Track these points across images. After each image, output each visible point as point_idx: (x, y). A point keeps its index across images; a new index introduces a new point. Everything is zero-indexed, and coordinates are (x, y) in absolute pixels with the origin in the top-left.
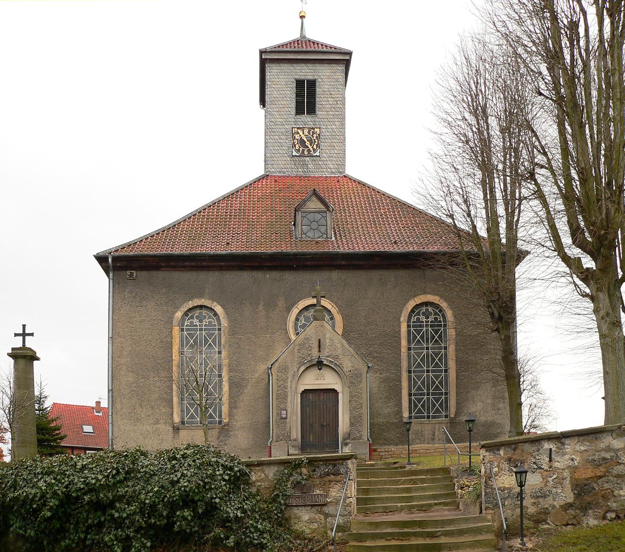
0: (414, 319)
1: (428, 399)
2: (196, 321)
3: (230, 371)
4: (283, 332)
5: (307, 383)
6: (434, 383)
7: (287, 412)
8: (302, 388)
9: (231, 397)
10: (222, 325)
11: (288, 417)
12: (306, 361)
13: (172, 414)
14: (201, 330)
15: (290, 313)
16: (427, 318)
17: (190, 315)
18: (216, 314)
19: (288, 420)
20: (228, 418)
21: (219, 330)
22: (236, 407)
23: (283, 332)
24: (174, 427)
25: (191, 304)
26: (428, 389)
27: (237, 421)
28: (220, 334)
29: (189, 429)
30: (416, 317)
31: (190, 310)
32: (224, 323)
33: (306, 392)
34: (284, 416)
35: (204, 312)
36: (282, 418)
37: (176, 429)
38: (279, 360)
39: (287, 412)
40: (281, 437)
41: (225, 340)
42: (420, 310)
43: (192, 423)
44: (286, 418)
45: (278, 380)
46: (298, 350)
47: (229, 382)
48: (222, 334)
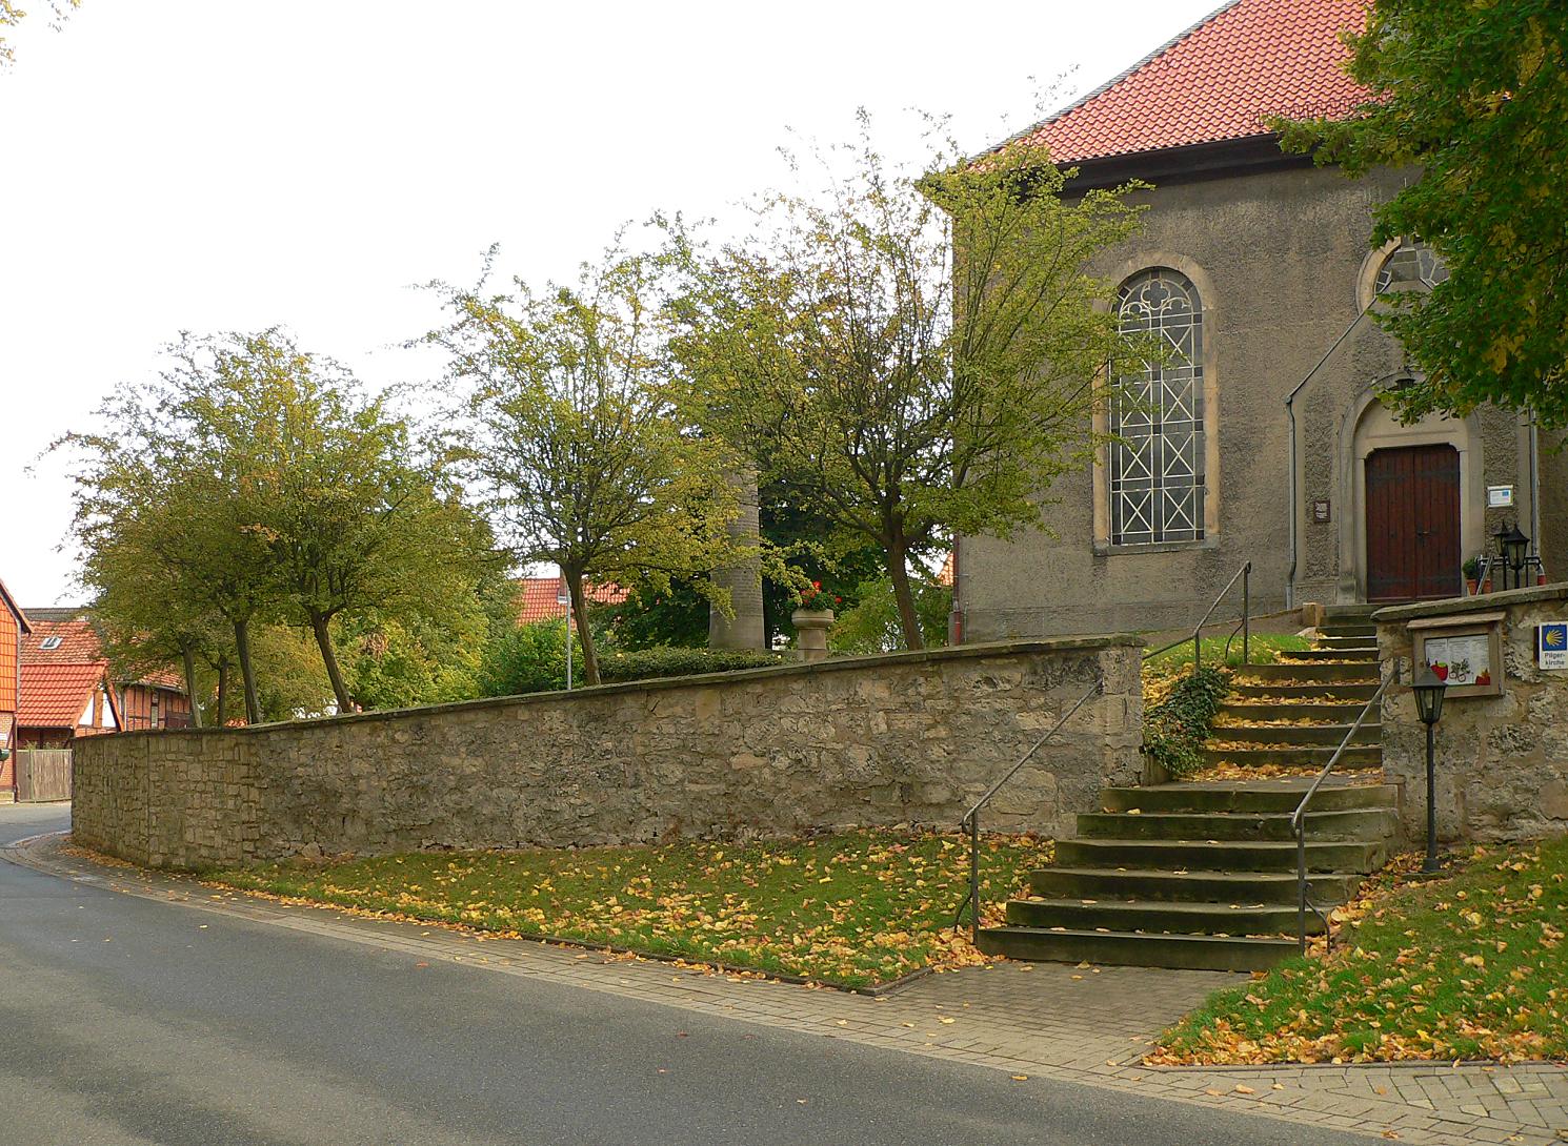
0: (1126, 310)
1: (1158, 493)
2: (1145, 306)
3: (1223, 412)
4: (1348, 311)
5: (1382, 433)
6: (1170, 455)
7: (1329, 506)
8: (1367, 447)
9: (1224, 474)
10: (1204, 309)
11: (1333, 517)
12: (1374, 382)
13: (1091, 522)
14: (1156, 323)
15: (1364, 263)
16: (1156, 304)
17: (1131, 292)
18: (1188, 284)
19: (1332, 524)
20: (1217, 524)
21: (1198, 319)
22: (1236, 498)
23: (1348, 311)
24: (1094, 552)
25: (1130, 268)
26: (1158, 473)
27: (1239, 531)
28: (1198, 330)
29: (1129, 552)
30: (1129, 305)
31: (1131, 280)
32: (1208, 305)
33: (1376, 455)
34: (1322, 516)
35: (1163, 282)
36: (1317, 521)
37: (1101, 557)
38: (1309, 387)
39: (1329, 506)
40: (1315, 568)
41: (1210, 342)
42: (1141, 288)
43: (1179, 536)
44: (1327, 521)
45: (1307, 431)
46: (1354, 355)
47: (1220, 440)
48: (1204, 329)
